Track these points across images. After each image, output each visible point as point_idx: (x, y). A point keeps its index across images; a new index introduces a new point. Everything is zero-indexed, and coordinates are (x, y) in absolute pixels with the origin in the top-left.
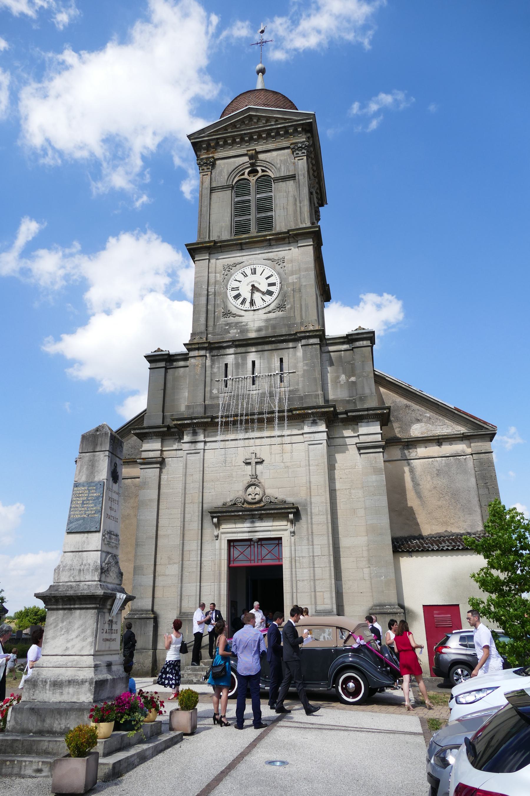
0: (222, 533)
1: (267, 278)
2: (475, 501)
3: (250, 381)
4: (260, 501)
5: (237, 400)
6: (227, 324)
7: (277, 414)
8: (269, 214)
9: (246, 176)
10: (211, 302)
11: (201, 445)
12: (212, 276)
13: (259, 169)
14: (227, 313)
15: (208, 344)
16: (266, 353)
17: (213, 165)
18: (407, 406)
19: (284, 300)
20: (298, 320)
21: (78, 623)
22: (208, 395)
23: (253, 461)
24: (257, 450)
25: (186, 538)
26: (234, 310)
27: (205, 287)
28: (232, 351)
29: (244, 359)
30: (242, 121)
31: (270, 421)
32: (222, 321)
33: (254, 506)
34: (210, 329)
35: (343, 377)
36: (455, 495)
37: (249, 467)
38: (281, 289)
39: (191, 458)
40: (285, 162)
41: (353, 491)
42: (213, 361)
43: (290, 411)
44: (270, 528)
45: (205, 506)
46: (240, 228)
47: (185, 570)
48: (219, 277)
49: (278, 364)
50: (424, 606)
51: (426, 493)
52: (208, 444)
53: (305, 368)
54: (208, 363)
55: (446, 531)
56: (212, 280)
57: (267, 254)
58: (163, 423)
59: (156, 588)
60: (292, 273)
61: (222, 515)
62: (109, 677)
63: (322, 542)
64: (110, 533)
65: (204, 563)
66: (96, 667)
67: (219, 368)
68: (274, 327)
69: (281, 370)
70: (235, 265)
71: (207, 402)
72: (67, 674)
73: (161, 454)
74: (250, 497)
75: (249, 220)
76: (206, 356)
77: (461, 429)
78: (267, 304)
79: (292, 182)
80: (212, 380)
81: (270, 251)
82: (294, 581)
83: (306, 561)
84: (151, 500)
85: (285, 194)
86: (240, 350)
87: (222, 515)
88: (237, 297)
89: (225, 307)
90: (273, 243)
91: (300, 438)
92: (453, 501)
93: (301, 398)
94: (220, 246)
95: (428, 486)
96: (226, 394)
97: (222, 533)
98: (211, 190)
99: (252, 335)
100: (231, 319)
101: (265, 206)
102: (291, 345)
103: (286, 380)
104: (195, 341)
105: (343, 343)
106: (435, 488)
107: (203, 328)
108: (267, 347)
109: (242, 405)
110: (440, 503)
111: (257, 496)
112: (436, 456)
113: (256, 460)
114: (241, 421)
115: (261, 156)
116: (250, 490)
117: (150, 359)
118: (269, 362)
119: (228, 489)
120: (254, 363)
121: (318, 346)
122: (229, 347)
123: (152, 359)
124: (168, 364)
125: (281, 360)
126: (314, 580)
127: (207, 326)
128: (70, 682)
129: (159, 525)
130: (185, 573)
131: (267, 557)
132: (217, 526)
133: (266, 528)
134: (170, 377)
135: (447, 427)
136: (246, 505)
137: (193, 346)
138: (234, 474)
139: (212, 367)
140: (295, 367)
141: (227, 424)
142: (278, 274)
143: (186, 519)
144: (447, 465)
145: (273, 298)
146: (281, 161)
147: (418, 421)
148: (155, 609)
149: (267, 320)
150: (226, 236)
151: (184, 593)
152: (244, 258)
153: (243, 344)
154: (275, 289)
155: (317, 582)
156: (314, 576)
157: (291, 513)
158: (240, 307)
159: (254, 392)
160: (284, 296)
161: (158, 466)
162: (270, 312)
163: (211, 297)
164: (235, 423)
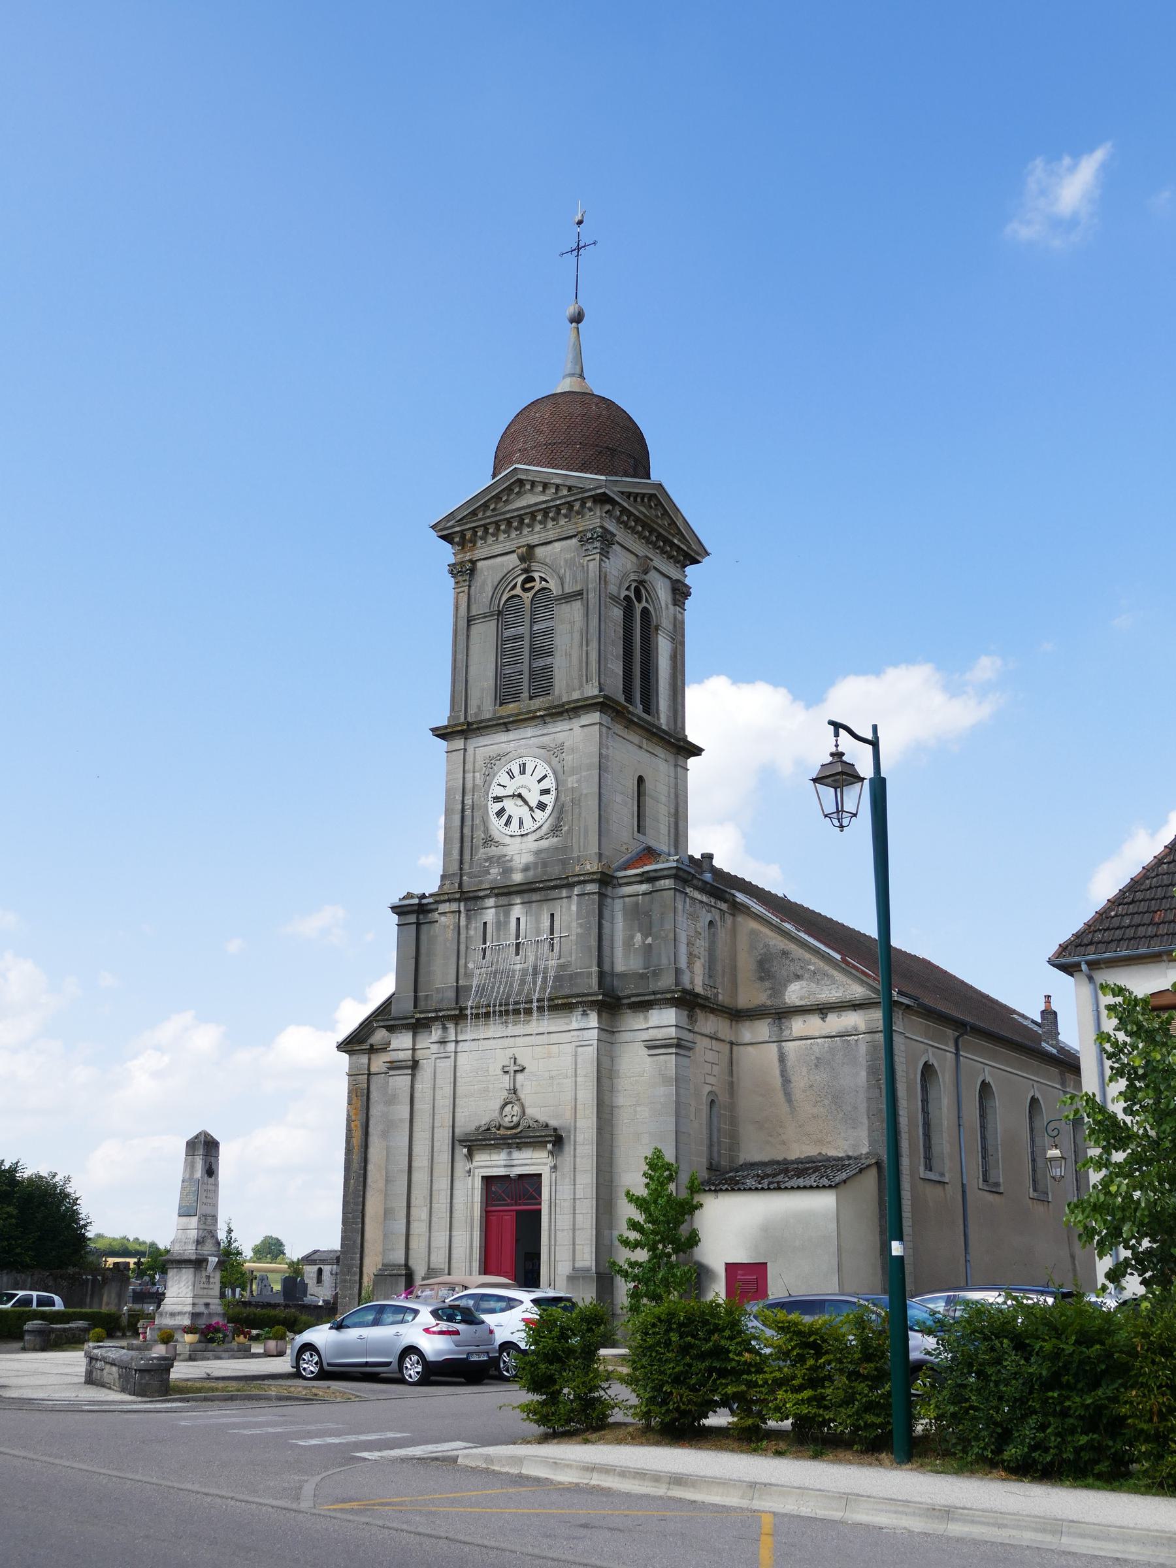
1: (539, 781)
2: (863, 1107)
3: (513, 949)
4: (518, 1125)
5: (495, 978)
6: (488, 859)
7: (535, 1004)
8: (548, 661)
9: (518, 591)
10: (468, 823)
11: (451, 1047)
12: (469, 776)
13: (536, 575)
14: (489, 841)
15: (466, 889)
16: (534, 905)
17: (472, 571)
18: (785, 953)
21: (184, 1278)
22: (462, 971)
23: (513, 1068)
24: (518, 1053)
25: (435, 1174)
26: (497, 836)
27: (459, 797)
28: (491, 902)
29: (507, 915)
30: (509, 489)
31: (528, 1012)
34: (466, 866)
35: (638, 937)
36: (837, 1098)
39: (441, 1064)
40: (570, 563)
41: (638, 1109)
42: (468, 918)
43: (550, 999)
44: (529, 1161)
45: (457, 1130)
46: (505, 692)
47: (434, 1215)
48: (479, 782)
49: (547, 923)
51: (798, 1095)
52: (461, 1044)
53: (579, 930)
54: (463, 922)
56: (469, 785)
57: (541, 739)
58: (415, 1007)
59: (411, 1237)
60: (573, 772)
61: (473, 1143)
62: (206, 1311)
63: (587, 1180)
64: (205, 1216)
65: (456, 1207)
66: (194, 1304)
67: (476, 928)
68: (545, 865)
69: (552, 933)
70: (500, 757)
72: (179, 1308)
73: (413, 1056)
74: (507, 1119)
76: (459, 912)
78: (539, 824)
79: (579, 603)
80: (467, 948)
81: (545, 732)
82: (553, 1232)
83: (567, 1205)
84: (401, 1120)
85: (569, 626)
86: (503, 900)
87: (473, 1143)
88: (500, 813)
89: (486, 830)
90: (548, 719)
92: (834, 1107)
93: (572, 977)
94: (478, 729)
95: (802, 1085)
96: (484, 970)
98: (469, 621)
99: (518, 877)
100: (493, 851)
101: (541, 649)
102: (564, 893)
103: (556, 947)
104: (446, 889)
105: (641, 882)
106: (811, 1086)
107: (455, 867)
108: (535, 896)
109: (498, 992)
110: (815, 1111)
112: (817, 1034)
113: (517, 1068)
114: (494, 1012)
116: (508, 1108)
117: (399, 910)
118: (538, 921)
119: (480, 1110)
120: (518, 919)
121: (596, 897)
123: (398, 910)
124: (421, 917)
125: (552, 915)
126: (574, 1230)
127: (461, 862)
128: (179, 1313)
129: (414, 1153)
130: (434, 1219)
132: (470, 1156)
133: (528, 1161)
134: (423, 937)
136: (502, 1132)
137: (442, 898)
138: (491, 1086)
139: (467, 928)
140: (569, 928)
141: (477, 1016)
142: (555, 773)
143: (435, 1149)
144: (832, 1050)
145: (546, 815)
147: (798, 977)
148: (411, 1263)
149: (538, 852)
151: (433, 1245)
152: (512, 745)
153: (505, 892)
154: (548, 799)
155: (577, 1233)
156: (574, 1225)
157: (549, 1142)
158: (503, 830)
159: (518, 965)
160: (560, 811)
161: (409, 1071)
162: (541, 839)
163: (468, 813)
164: (487, 1015)
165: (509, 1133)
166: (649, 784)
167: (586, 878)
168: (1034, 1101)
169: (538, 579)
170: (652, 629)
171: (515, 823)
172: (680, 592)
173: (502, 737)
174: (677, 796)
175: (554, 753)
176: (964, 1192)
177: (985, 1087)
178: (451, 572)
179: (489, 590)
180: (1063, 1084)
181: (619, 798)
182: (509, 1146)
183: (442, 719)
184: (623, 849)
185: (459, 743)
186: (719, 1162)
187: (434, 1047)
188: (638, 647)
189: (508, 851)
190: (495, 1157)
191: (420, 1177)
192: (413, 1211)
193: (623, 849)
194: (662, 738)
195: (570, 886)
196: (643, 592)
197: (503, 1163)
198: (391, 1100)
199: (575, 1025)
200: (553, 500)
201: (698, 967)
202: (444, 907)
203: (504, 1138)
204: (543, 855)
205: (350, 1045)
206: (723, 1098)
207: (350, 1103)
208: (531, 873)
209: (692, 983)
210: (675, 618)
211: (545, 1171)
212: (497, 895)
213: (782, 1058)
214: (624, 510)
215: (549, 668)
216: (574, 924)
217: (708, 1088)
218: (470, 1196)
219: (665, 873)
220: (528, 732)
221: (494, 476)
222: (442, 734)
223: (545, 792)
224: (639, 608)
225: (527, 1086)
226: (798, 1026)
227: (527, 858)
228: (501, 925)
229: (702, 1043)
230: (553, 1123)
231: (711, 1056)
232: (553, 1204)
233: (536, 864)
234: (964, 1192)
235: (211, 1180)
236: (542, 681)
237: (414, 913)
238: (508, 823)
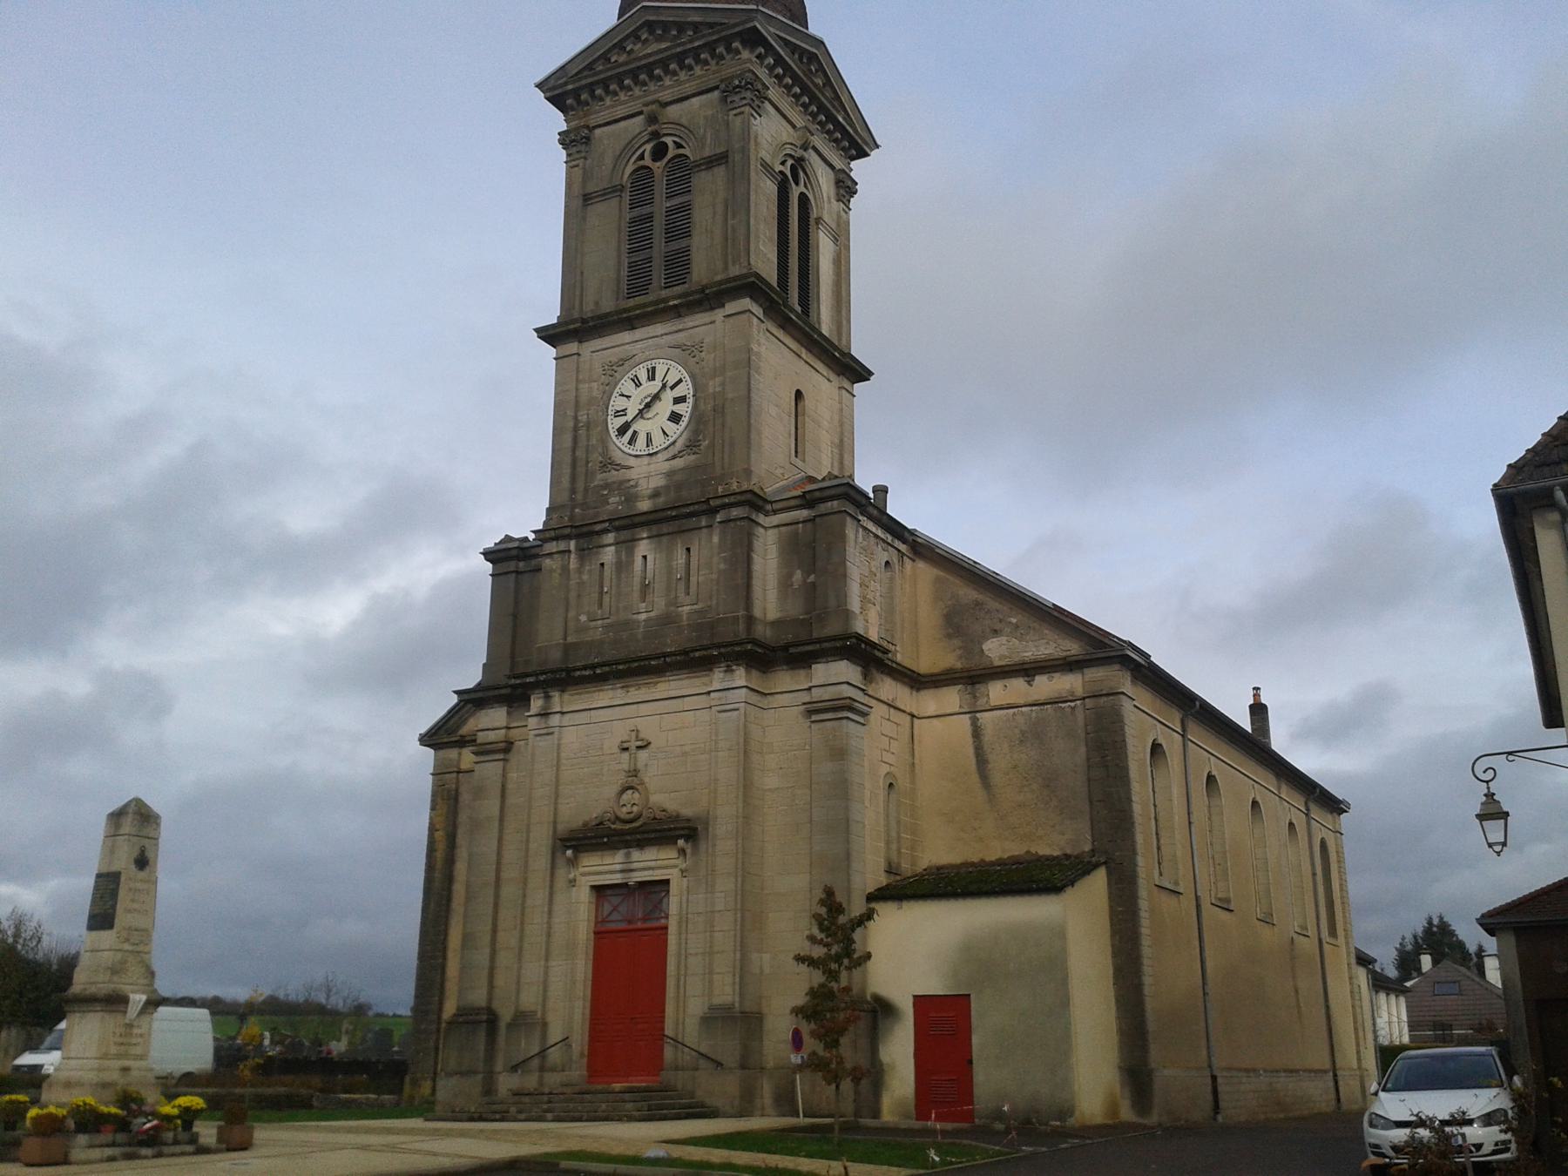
0: (584, 874)
4: (639, 816)
6: (607, 486)
9: (647, 161)
10: (582, 442)
13: (669, 140)
14: (609, 464)
17: (587, 140)
18: (977, 604)
19: (696, 432)
20: (718, 471)
22: (571, 624)
23: (633, 744)
26: (618, 457)
28: (610, 538)
29: (631, 553)
32: (600, 478)
33: (628, 826)
35: (798, 575)
37: (626, 755)
38: (695, 407)
42: (582, 559)
46: (638, 279)
50: (915, 997)
51: (997, 778)
53: (722, 566)
55: (1028, 852)
68: (679, 487)
70: (622, 362)
71: (570, 639)
74: (624, 810)
75: (649, 260)
77: (1072, 648)
79: (722, 168)
86: (625, 535)
89: (605, 451)
91: (702, 701)
97: (584, 874)
99: (644, 505)
100: (614, 476)
101: (679, 225)
106: (1015, 767)
108: (665, 528)
111: (635, 809)
112: (1022, 702)
115: (673, 111)
116: (628, 795)
118: (669, 559)
119: (592, 798)
122: (606, 531)
125: (688, 550)
131: (612, 918)
132: (573, 863)
133: (651, 863)
135: (1049, 646)
136: (618, 826)
139: (580, 571)
142: (693, 377)
146: (706, 118)
147: (996, 632)
149: (670, 474)
150: (608, 305)
152: (639, 345)
160: (698, 417)
162: (674, 457)
165: (628, 826)
166: (809, 402)
167: (732, 499)
168: (1255, 804)
169: (671, 145)
170: (812, 222)
171: (641, 439)
172: (846, 188)
173: (626, 336)
174: (842, 425)
175: (687, 353)
176: (1198, 906)
177: (1211, 779)
178: (562, 142)
179: (609, 161)
180: (1279, 789)
181: (773, 411)
182: (627, 845)
183: (551, 316)
184: (779, 472)
185: (572, 347)
186: (899, 864)
187: (533, 722)
188: (796, 218)
189: (633, 474)
190: (608, 860)
191: (509, 891)
192: (501, 935)
193: (779, 472)
194: (825, 351)
195: (714, 511)
196: (802, 174)
197: (618, 867)
198: (479, 792)
199: (716, 686)
200: (691, 41)
201: (873, 614)
202: (552, 547)
203: (622, 833)
204: (676, 478)
205: (431, 739)
206: (903, 782)
207: (433, 809)
208: (661, 499)
209: (867, 628)
210: (839, 217)
211: (673, 875)
212: (617, 529)
213: (977, 733)
214: (780, 61)
215: (686, 251)
216: (715, 559)
217: (885, 769)
218: (577, 913)
219: (833, 492)
220: (659, 329)
221: (620, 17)
222: (549, 335)
223: (679, 400)
224: (795, 191)
225: (653, 768)
226: (997, 692)
227: (658, 482)
228: (623, 566)
229: (879, 711)
230: (687, 812)
231: (888, 728)
232: (684, 920)
233: (667, 487)
234: (1198, 906)
235: (142, 875)
236: (678, 264)
237: (509, 559)
238: (632, 441)
